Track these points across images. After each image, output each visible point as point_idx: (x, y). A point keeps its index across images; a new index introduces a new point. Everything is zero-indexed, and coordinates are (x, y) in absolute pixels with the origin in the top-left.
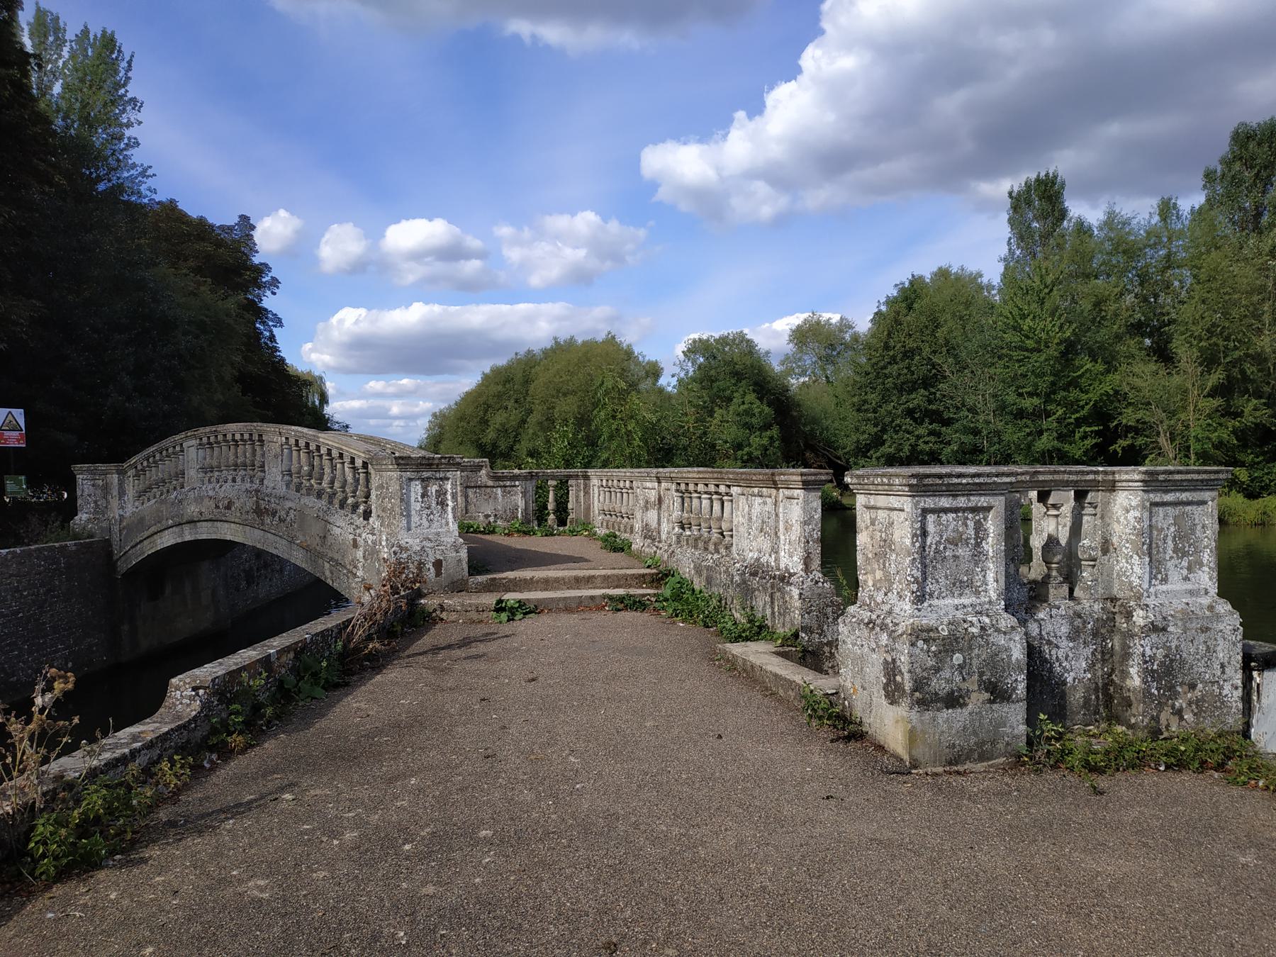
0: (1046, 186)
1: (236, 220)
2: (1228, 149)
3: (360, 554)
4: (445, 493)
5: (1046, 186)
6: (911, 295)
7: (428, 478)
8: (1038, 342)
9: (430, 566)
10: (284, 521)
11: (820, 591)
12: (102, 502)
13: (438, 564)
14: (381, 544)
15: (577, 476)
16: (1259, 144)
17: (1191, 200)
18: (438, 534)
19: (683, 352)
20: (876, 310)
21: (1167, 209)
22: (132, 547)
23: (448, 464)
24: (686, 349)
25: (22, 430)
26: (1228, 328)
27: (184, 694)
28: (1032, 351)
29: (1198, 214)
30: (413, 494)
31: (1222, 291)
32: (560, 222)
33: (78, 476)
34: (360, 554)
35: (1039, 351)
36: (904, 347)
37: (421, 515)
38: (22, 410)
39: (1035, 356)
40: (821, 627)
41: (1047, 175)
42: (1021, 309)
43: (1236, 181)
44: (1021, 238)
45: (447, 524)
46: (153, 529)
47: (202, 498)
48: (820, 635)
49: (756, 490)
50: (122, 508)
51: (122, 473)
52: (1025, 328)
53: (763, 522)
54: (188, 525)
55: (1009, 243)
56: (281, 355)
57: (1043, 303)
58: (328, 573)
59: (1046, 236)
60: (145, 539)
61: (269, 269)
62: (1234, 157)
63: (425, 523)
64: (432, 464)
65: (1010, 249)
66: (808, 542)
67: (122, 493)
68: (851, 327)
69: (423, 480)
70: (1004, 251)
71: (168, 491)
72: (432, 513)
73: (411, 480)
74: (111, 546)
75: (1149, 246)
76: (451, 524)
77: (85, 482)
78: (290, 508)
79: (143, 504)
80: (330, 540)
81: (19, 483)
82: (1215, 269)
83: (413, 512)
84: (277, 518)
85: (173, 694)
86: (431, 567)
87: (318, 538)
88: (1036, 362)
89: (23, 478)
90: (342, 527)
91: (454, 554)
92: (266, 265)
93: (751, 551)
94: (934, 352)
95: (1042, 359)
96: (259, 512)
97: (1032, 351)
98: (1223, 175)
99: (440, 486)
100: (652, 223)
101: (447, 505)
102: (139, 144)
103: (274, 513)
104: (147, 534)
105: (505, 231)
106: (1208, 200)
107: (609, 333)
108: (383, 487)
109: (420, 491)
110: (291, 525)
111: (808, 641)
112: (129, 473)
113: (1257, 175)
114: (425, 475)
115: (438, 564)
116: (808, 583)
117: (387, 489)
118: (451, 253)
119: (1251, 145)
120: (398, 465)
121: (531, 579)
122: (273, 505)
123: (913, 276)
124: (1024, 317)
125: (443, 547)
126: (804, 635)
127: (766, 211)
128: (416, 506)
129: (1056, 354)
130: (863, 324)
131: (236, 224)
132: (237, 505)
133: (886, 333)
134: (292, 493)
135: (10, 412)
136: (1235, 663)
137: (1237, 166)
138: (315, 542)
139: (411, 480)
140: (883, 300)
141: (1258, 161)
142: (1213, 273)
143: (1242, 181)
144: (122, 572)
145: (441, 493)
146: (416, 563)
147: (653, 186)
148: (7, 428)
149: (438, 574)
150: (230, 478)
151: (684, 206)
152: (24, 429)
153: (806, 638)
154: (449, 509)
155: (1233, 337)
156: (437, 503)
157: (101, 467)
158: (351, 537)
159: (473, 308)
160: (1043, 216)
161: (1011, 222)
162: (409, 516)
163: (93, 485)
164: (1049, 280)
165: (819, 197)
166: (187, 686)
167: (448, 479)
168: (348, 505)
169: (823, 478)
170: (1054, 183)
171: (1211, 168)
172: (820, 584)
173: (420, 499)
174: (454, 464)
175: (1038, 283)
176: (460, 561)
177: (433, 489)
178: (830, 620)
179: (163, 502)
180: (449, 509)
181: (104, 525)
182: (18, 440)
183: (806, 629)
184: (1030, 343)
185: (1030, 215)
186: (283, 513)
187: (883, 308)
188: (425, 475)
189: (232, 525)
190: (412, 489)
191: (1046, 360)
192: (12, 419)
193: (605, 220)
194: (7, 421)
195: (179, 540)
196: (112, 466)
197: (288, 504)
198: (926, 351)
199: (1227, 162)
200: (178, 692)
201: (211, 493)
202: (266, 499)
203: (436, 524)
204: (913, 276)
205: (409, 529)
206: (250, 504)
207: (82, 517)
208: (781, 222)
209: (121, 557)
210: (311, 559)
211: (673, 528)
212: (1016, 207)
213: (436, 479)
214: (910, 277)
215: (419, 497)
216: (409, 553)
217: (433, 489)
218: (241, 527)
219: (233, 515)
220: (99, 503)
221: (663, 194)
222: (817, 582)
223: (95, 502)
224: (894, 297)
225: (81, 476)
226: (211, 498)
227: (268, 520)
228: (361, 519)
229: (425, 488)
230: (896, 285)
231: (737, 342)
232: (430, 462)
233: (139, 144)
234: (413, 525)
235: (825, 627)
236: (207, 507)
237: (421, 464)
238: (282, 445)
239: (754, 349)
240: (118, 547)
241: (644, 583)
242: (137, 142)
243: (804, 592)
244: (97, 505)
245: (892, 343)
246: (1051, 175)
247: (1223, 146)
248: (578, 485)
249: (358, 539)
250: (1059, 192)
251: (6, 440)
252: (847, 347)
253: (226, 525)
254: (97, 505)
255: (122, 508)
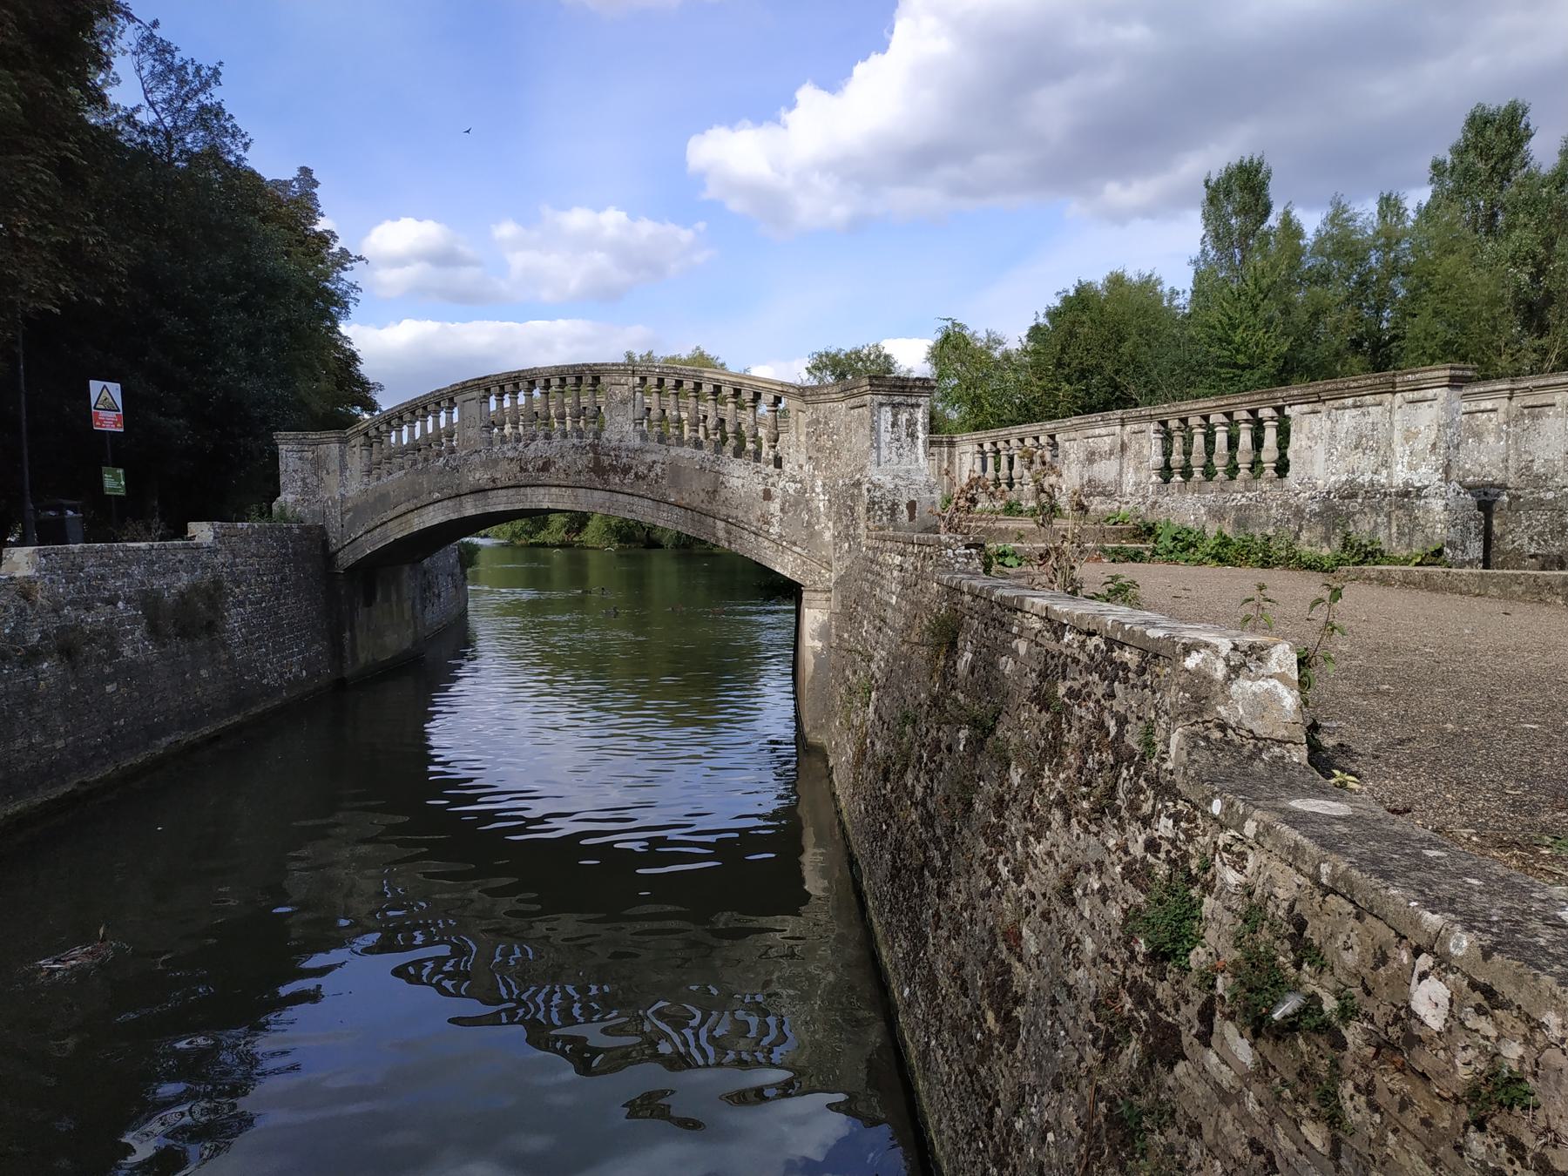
0: (1249, 174)
1: (296, 173)
2: (1461, 136)
3: (775, 507)
4: (915, 424)
5: (1249, 174)
6: (1079, 303)
7: (900, 404)
8: (1251, 358)
9: (903, 507)
10: (644, 478)
11: (1463, 502)
12: (311, 480)
13: (912, 506)
14: (814, 491)
15: (942, 442)
16: (1498, 131)
17: (1417, 197)
18: (908, 471)
19: (807, 369)
20: (1033, 324)
21: (1389, 205)
22: (366, 533)
23: (923, 387)
24: (809, 366)
25: (118, 410)
26: (1465, 345)
27: (957, 552)
28: (1243, 368)
29: (1426, 213)
30: (883, 423)
31: (1460, 301)
32: (578, 219)
33: (280, 447)
34: (775, 507)
35: (1251, 367)
36: (1082, 363)
37: (890, 448)
38: (119, 385)
39: (1247, 374)
40: (1463, 543)
41: (1251, 161)
42: (1230, 318)
43: (1468, 174)
44: (1217, 237)
45: (917, 460)
46: (402, 508)
47: (496, 462)
48: (1463, 552)
49: (1350, 401)
50: (344, 485)
51: (344, 441)
52: (1237, 339)
53: (1361, 436)
54: (472, 496)
55: (1203, 242)
56: (352, 347)
57: (1256, 311)
58: (721, 534)
59: (1245, 235)
60: (391, 520)
61: (335, 237)
62: (1468, 146)
63: (895, 458)
64: (906, 387)
65: (1203, 251)
66: (1449, 448)
67: (343, 467)
68: (1000, 343)
69: (894, 406)
70: (1196, 250)
71: (426, 460)
72: (901, 446)
73: (881, 405)
74: (325, 534)
75: (1375, 247)
76: (921, 460)
77: (289, 454)
78: (654, 462)
79: (379, 479)
80: (724, 493)
81: (116, 477)
82: (1453, 276)
83: (883, 445)
84: (632, 475)
85: (944, 552)
86: (905, 509)
87: (702, 495)
88: (1249, 380)
89: (120, 471)
90: (740, 477)
91: (928, 495)
92: (332, 233)
93: (1333, 474)
94: (1117, 372)
95: (1257, 376)
96: (599, 469)
97: (1243, 368)
98: (1453, 168)
99: (911, 414)
100: (701, 226)
101: (918, 438)
102: (119, 82)
103: (626, 470)
104: (391, 514)
105: (506, 230)
106: (1434, 196)
107: (698, 348)
108: (819, 423)
109: (891, 419)
110: (656, 482)
111: (1452, 558)
112: (353, 443)
113: (1493, 168)
114: (897, 399)
115: (912, 506)
116: (1451, 494)
117: (826, 423)
118: (444, 258)
119: (1489, 132)
120: (871, 385)
121: (1006, 528)
122: (624, 460)
123: (1080, 282)
124: (1234, 327)
125: (917, 487)
126: (1449, 551)
127: (840, 212)
128: (886, 437)
129: (1272, 370)
130: (1014, 337)
131: (295, 179)
132: (561, 464)
133: (1059, 348)
134: (653, 445)
135: (105, 387)
136: (1011, 895)
137: (1471, 157)
138: (698, 500)
139: (881, 405)
140: (1042, 311)
141: (1496, 151)
142: (1449, 281)
143: (1477, 174)
144: (346, 565)
145: (911, 423)
146: (890, 504)
147: (700, 179)
148: (102, 407)
149: (912, 518)
150: (541, 434)
151: (735, 205)
152: (121, 408)
153: (1451, 555)
154: (920, 442)
155: (1471, 355)
156: (908, 435)
157: (313, 436)
158: (761, 487)
159: (476, 324)
160: (1244, 211)
161: (1206, 217)
162: (878, 448)
163: (300, 459)
164: (1265, 282)
165: (924, 197)
166: (960, 544)
167: (918, 406)
168: (749, 451)
169: (1469, 373)
170: (1258, 172)
171: (1440, 158)
172: (1462, 495)
173: (890, 429)
174: (927, 388)
175: (1252, 287)
176: (934, 503)
177: (904, 417)
178: (1472, 535)
179: (424, 471)
180: (920, 442)
181: (317, 507)
182: (115, 423)
183: (1451, 544)
184: (1241, 359)
185: (1230, 209)
186: (642, 469)
187: (1043, 320)
188: (897, 399)
189: (553, 489)
190: (882, 417)
191: (1261, 378)
192: (108, 396)
193: (633, 217)
194: (102, 398)
195: (454, 516)
196: (332, 434)
197: (649, 458)
198: (1109, 369)
199: (1459, 151)
200: (949, 551)
201: (510, 454)
202: (612, 453)
203: (905, 459)
204: (1080, 282)
205: (879, 465)
206: (585, 461)
207: (287, 497)
208: (858, 226)
209: (344, 547)
210: (693, 520)
211: (1150, 477)
212: (1212, 200)
213: (908, 405)
214: (1076, 284)
215: (889, 427)
216: (883, 490)
217: (904, 417)
218: (569, 491)
219: (551, 476)
220: (308, 481)
221: (711, 192)
222: (1459, 493)
223: (303, 480)
224: (1057, 308)
225: (285, 447)
226: (512, 460)
227: (615, 479)
228: (772, 466)
229: (895, 416)
230: (1058, 293)
231: (872, 357)
232: (905, 383)
233: (119, 82)
234: (882, 460)
235: (1468, 543)
236: (503, 473)
237: (895, 386)
238: (634, 387)
239: (893, 365)
240: (338, 536)
241: (1123, 539)
242: (118, 79)
243: (1450, 503)
244: (306, 484)
245: (1066, 359)
246: (1255, 162)
247: (1455, 132)
248: (940, 454)
249: (773, 489)
250: (1264, 183)
251: (102, 421)
252: (997, 365)
253: (542, 491)
254: (306, 484)
255: (344, 485)
